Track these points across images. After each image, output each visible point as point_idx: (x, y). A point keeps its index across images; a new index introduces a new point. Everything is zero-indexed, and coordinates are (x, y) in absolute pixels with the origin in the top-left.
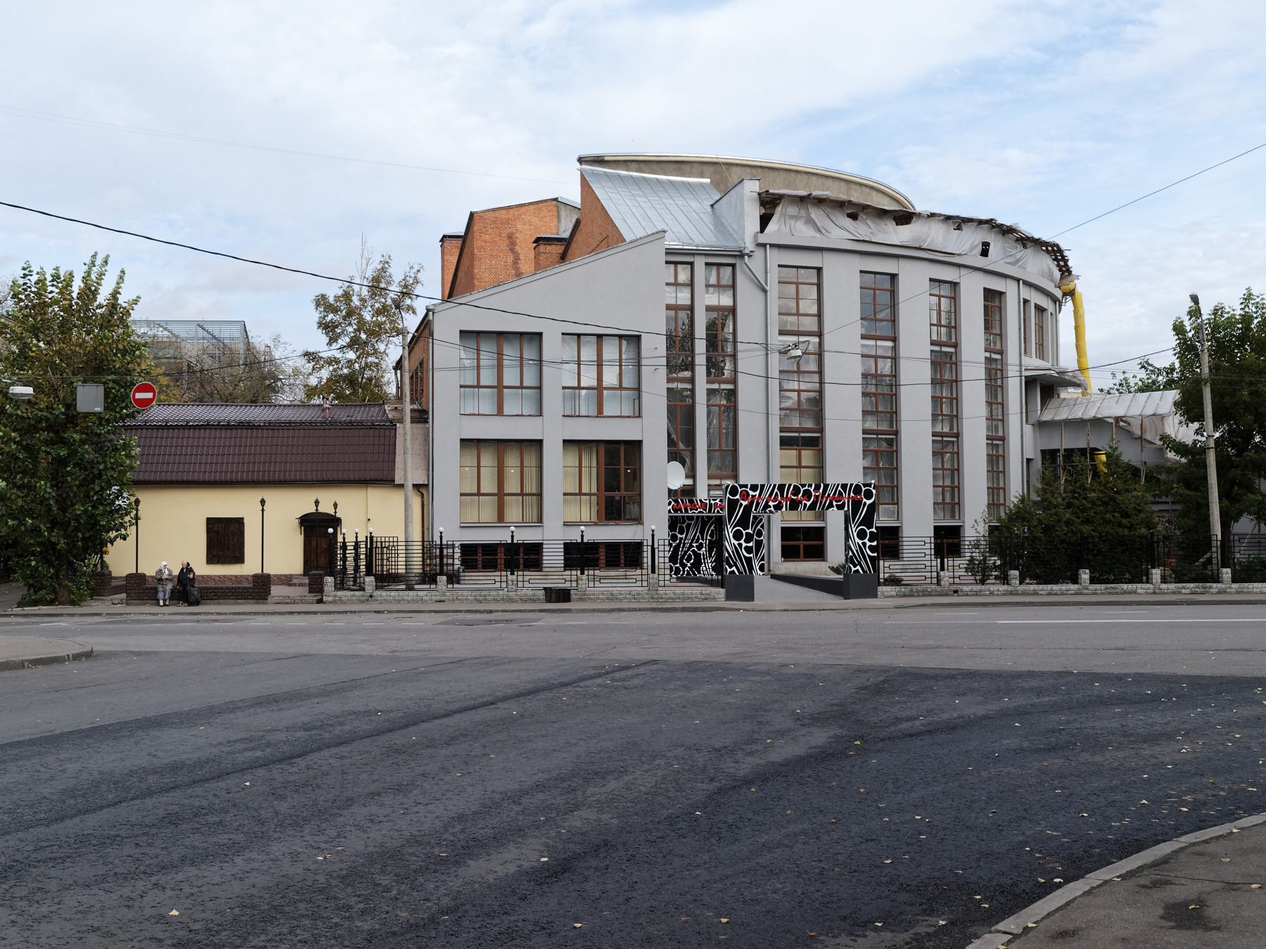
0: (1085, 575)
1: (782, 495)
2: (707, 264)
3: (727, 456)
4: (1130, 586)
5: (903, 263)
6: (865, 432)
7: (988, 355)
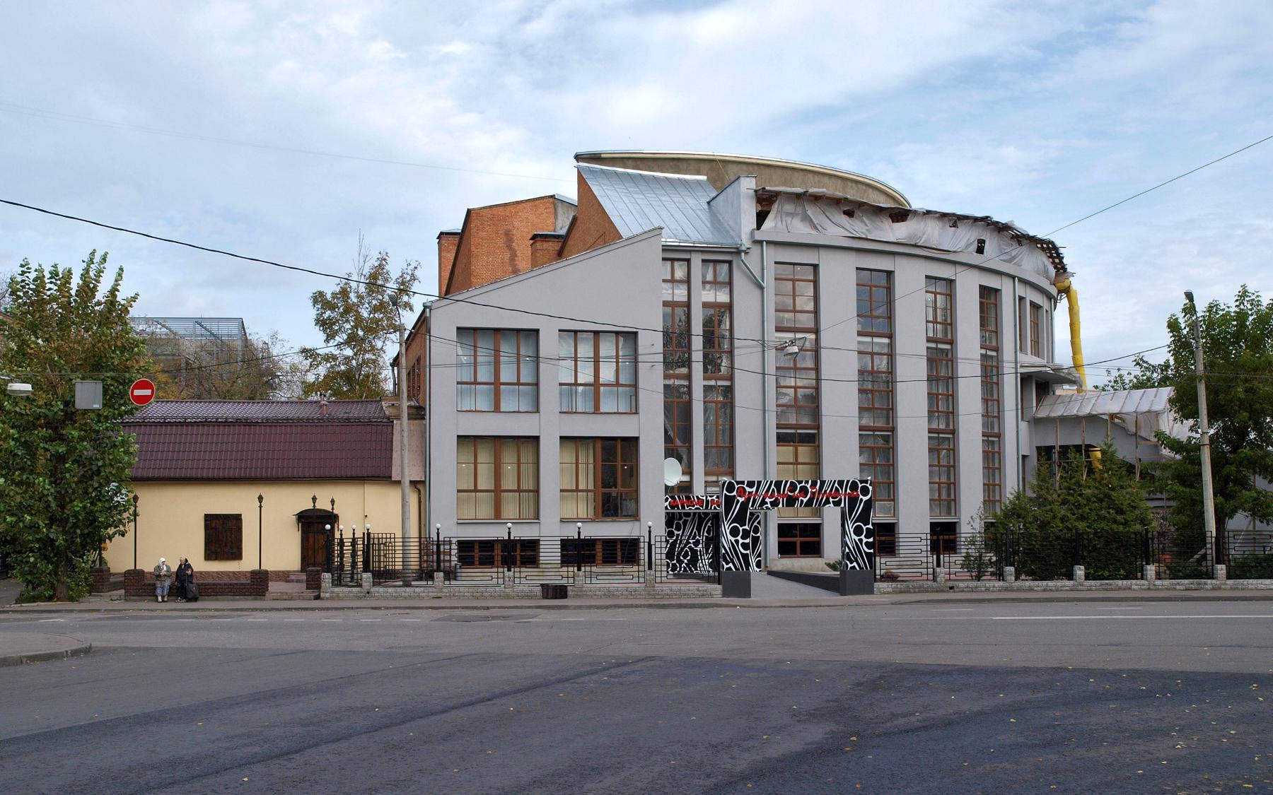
0: (1080, 571)
1: (779, 492)
2: (703, 261)
3: (723, 453)
5: (899, 260)
7: (983, 351)
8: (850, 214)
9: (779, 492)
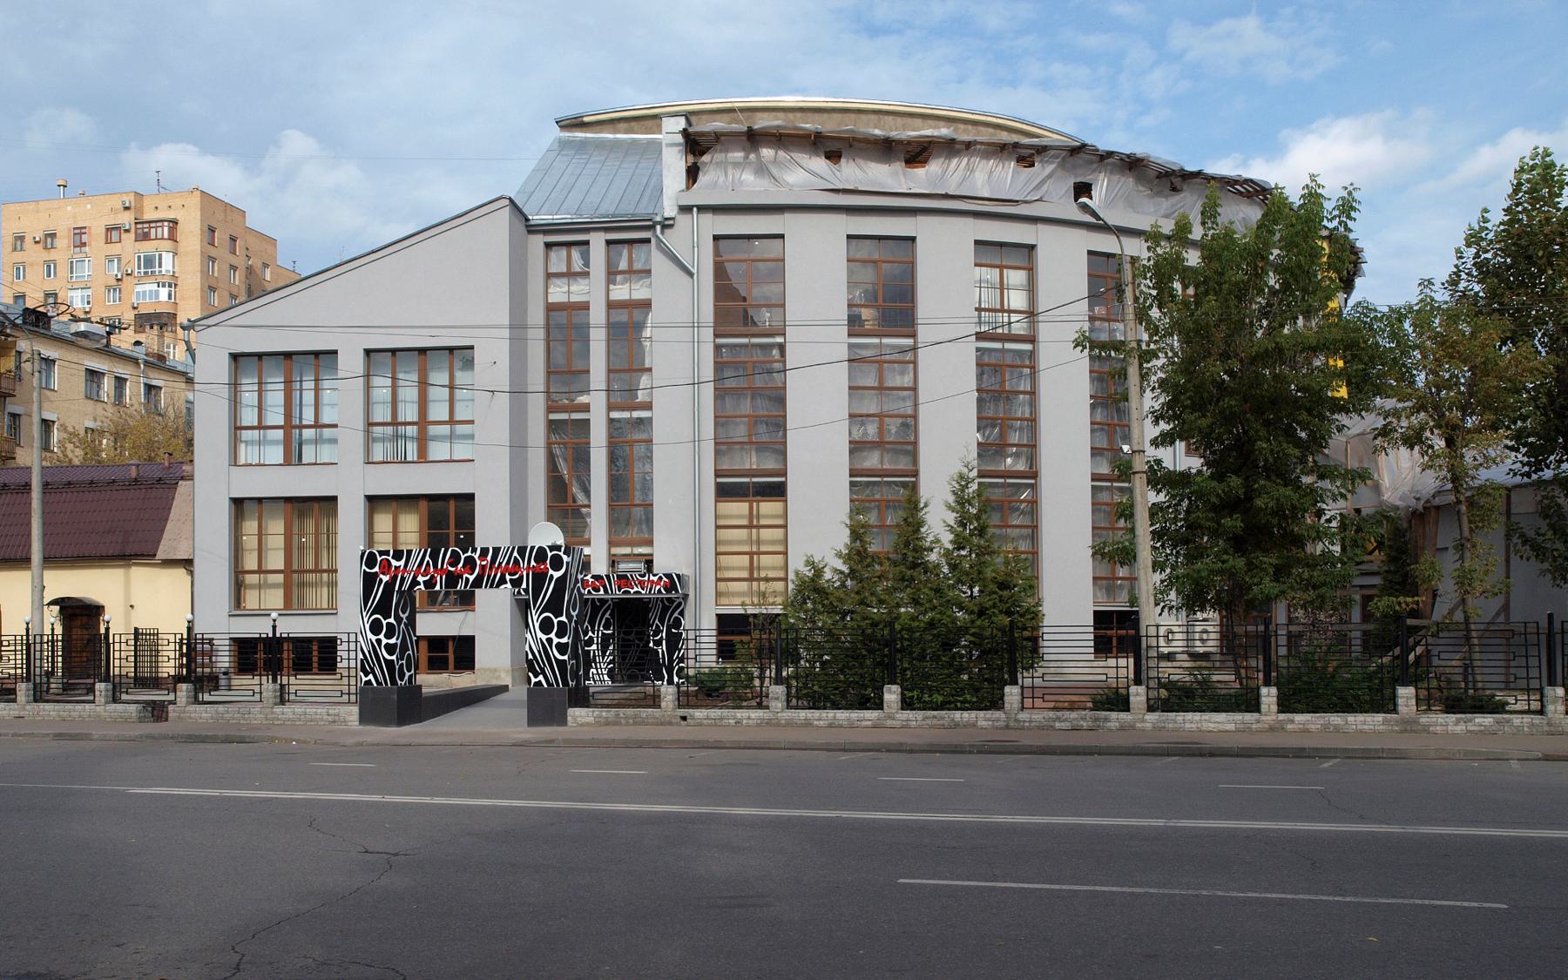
0: (892, 695)
1: (435, 565)
2: (609, 242)
4: (966, 714)
5: (922, 220)
6: (1095, 477)
8: (833, 156)
9: (435, 565)
